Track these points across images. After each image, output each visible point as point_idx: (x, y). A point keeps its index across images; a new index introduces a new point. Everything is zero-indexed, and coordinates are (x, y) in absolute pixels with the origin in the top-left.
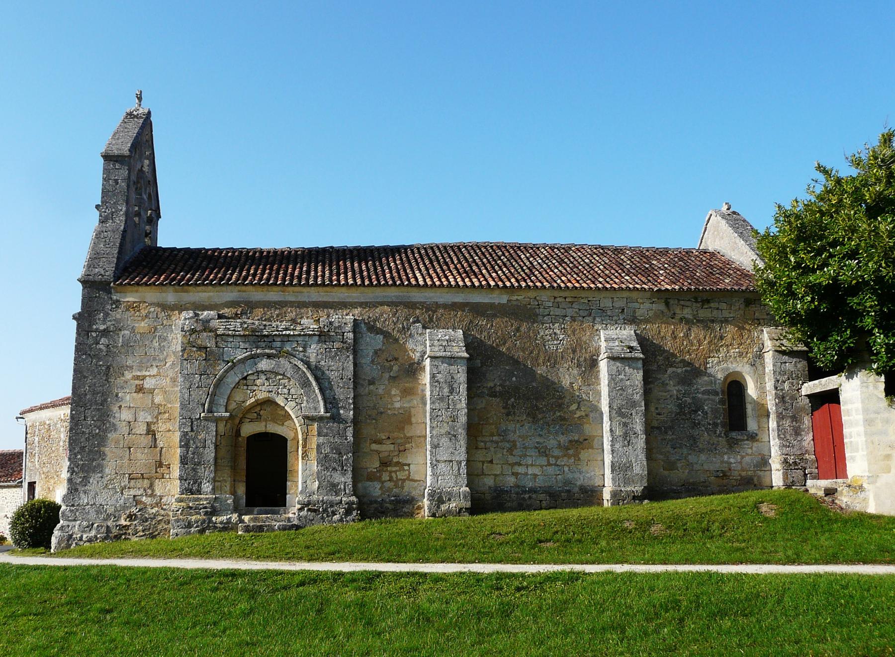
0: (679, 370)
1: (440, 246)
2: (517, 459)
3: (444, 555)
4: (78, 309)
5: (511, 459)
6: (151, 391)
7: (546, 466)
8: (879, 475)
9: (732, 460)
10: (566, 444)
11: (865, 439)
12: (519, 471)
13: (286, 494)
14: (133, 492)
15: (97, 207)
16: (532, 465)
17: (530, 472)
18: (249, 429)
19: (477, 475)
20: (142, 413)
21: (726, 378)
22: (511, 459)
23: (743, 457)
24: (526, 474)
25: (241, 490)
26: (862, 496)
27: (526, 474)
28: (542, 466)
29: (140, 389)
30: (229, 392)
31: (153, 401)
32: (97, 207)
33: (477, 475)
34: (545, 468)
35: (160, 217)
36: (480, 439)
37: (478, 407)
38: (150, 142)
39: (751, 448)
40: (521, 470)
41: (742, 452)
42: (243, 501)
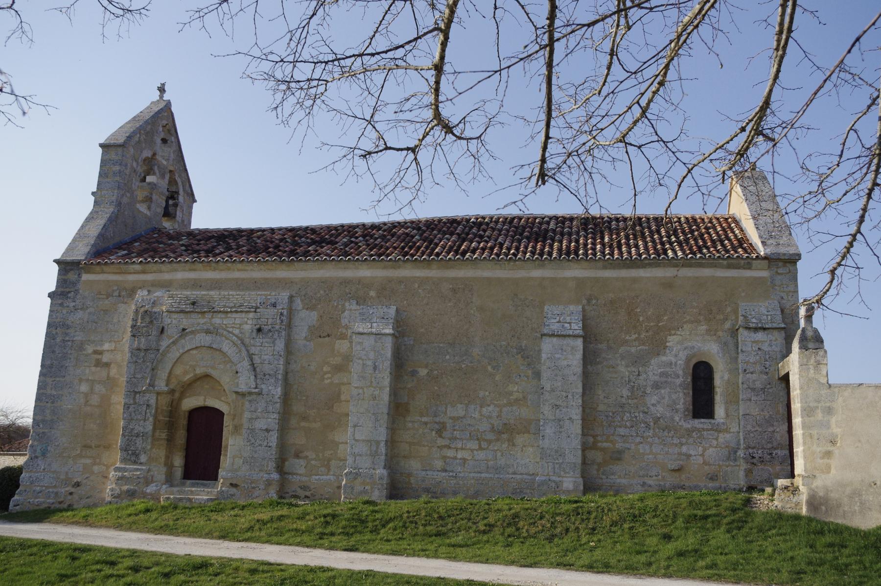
0: (633, 350)
1: (683, 219)
2: (447, 442)
3: (74, 520)
4: (53, 288)
5: (441, 442)
6: (107, 365)
7: (477, 450)
8: (817, 475)
9: (692, 452)
10: (500, 428)
11: (802, 432)
12: (448, 455)
13: (218, 467)
14: (84, 461)
15: (93, 193)
16: (462, 449)
17: (459, 456)
18: (190, 403)
19: (405, 457)
20: (97, 386)
21: (688, 359)
22: (441, 442)
23: (705, 450)
24: (455, 458)
25: (178, 461)
26: (794, 500)
27: (455, 458)
28: (472, 450)
29: (98, 363)
30: (171, 366)
31: (108, 374)
32: (93, 193)
33: (405, 457)
34: (475, 452)
35: (195, 201)
36: (408, 419)
37: (409, 386)
38: (173, 130)
39: (717, 439)
40: (450, 453)
41: (704, 443)
42: (179, 473)
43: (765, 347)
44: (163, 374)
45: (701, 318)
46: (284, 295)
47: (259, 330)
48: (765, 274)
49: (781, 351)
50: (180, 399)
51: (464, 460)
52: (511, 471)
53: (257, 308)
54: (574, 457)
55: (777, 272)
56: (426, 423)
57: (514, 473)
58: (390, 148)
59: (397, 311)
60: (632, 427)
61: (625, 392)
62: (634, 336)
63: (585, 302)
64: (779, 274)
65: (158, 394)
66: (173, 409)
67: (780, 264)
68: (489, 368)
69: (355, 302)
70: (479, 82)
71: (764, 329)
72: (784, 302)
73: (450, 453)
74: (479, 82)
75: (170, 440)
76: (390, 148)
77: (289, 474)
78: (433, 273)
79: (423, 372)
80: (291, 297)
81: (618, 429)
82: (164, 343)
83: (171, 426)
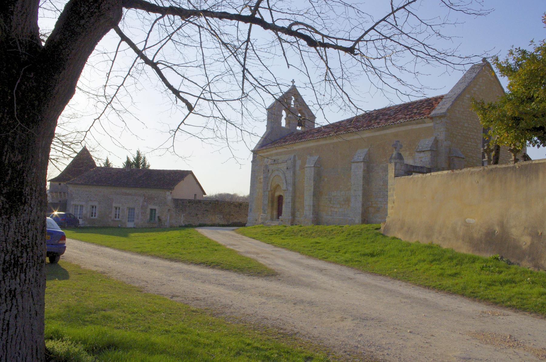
17: (335, 211)
40: (333, 209)
43: (423, 160)
44: (269, 185)
45: (407, 149)
46: (292, 156)
47: (287, 168)
48: (431, 124)
49: (429, 161)
50: (274, 193)
51: (336, 212)
52: (348, 216)
53: (287, 161)
54: (360, 211)
55: (436, 123)
56: (327, 198)
57: (349, 217)
58: (237, 99)
59: (319, 157)
60: (383, 197)
61: (381, 183)
62: (385, 159)
63: (370, 147)
64: (437, 123)
65: (269, 191)
66: (273, 196)
67: (438, 118)
68: (343, 176)
69: (309, 156)
70: (271, 73)
71: (423, 151)
72: (439, 136)
73: (333, 209)
74: (271, 73)
75: (272, 206)
76: (237, 99)
77: (297, 217)
78: (328, 141)
79: (326, 179)
80: (295, 156)
81: (379, 199)
82: (269, 174)
83: (272, 202)
